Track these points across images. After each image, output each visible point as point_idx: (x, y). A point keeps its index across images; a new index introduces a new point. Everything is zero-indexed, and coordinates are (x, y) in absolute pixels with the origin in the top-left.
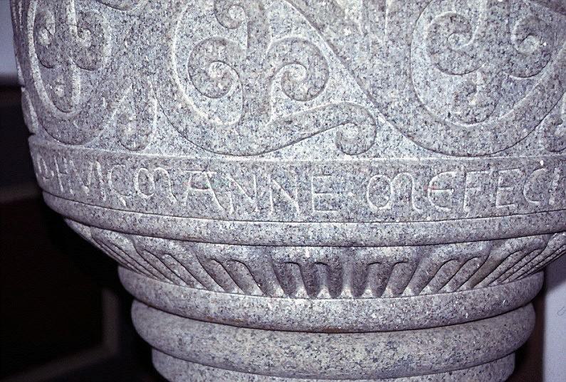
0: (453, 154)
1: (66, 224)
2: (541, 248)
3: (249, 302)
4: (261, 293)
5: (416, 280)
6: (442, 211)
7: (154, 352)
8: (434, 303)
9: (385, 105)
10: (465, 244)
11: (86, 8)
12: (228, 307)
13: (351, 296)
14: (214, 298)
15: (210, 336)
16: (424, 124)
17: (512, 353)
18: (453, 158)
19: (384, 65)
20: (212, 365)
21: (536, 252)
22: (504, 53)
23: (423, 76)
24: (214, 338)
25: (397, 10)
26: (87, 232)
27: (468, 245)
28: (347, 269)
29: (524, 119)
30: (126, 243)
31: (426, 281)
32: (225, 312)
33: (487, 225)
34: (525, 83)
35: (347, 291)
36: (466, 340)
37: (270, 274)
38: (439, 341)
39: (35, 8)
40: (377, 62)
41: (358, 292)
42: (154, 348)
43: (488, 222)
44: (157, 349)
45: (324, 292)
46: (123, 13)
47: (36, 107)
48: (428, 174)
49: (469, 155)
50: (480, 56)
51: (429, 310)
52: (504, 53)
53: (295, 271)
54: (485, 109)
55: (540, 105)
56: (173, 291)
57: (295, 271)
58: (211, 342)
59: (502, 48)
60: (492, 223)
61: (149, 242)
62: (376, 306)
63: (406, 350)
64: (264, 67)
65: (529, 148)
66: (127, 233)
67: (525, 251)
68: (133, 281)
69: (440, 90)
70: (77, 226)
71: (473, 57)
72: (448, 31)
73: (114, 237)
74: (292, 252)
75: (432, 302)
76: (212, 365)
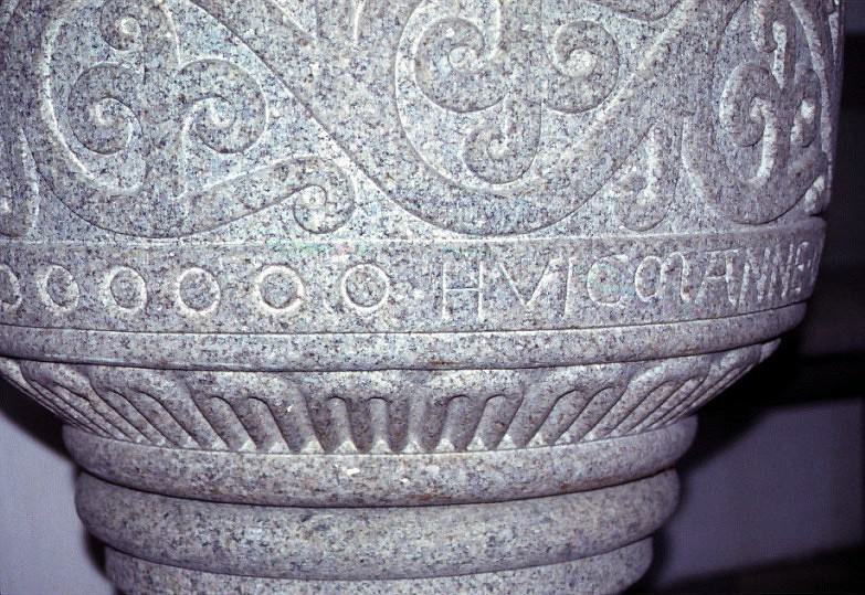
2: (620, 386)
4: (353, 447)
5: (485, 424)
9: (184, 263)
11: (570, 15)
12: (600, 460)
13: (388, 450)
15: (541, 518)
17: (649, 536)
20: (195, 565)
21: (666, 389)
24: (548, 520)
25: (535, 134)
28: (418, 409)
31: (504, 426)
32: (595, 469)
36: (594, 516)
37: (303, 420)
39: (54, 126)
41: (397, 445)
42: (108, 545)
46: (643, 26)
53: (338, 410)
57: (338, 410)
58: (547, 525)
62: (500, 459)
67: (675, 381)
76: (195, 565)
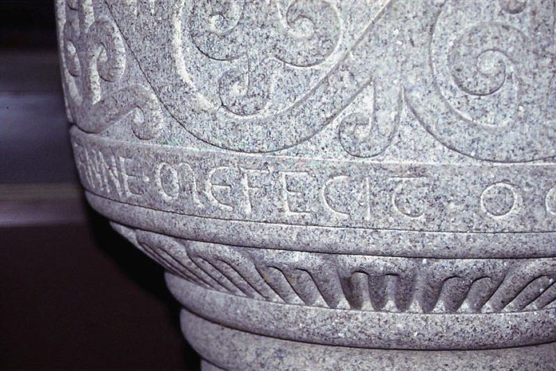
0: (224, 147)
1: (109, 225)
3: (316, 314)
6: (225, 208)
7: (203, 363)
8: (309, 316)
10: (277, 251)
14: (255, 308)
16: (191, 112)
18: (224, 151)
19: (153, 47)
22: (268, 37)
23: (192, 61)
26: (131, 235)
27: (280, 253)
28: (420, 284)
29: (302, 115)
30: (179, 249)
33: (281, 232)
34: (309, 73)
35: (415, 306)
38: (333, 361)
40: (148, 43)
43: (284, 229)
44: (208, 362)
45: (367, 305)
47: (69, 101)
48: (203, 166)
49: (241, 151)
50: (240, 40)
51: (303, 323)
52: (268, 37)
54: (252, 99)
55: (324, 99)
56: (216, 299)
57: (390, 282)
59: (265, 31)
60: (289, 231)
61: (200, 246)
63: (292, 363)
64: (533, 89)
65: (326, 149)
66: (180, 238)
68: (179, 287)
69: (211, 77)
70: (124, 231)
71: (232, 41)
72: (206, 12)
73: (156, 238)
74: (359, 260)
75: (306, 315)
